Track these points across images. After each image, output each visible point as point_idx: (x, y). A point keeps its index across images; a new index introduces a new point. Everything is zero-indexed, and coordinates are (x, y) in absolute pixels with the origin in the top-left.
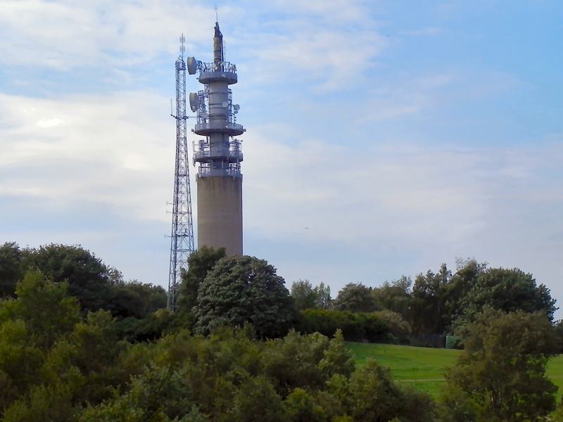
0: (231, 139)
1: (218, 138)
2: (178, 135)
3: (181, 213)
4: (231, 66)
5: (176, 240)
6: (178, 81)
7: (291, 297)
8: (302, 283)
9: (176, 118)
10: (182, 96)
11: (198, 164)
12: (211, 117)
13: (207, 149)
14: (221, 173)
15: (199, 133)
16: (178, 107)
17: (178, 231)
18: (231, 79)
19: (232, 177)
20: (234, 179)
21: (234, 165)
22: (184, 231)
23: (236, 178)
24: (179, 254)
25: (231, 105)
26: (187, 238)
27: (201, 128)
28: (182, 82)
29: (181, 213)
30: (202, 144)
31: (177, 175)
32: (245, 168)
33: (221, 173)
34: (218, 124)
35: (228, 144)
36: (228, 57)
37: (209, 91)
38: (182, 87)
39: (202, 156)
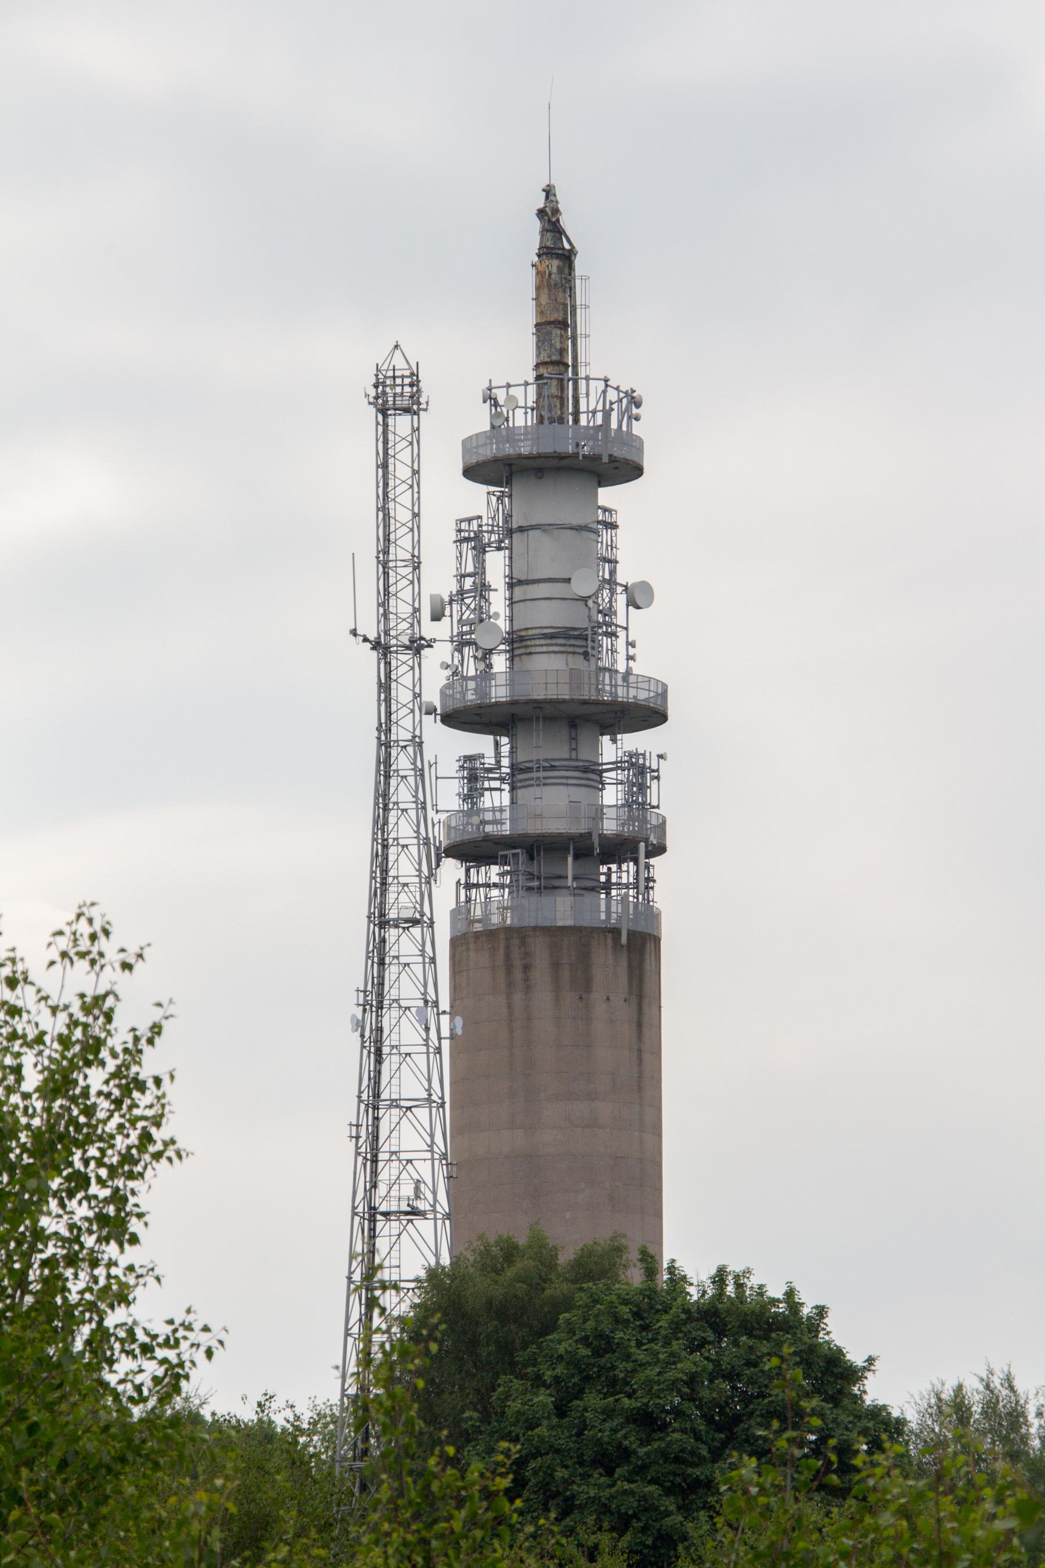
0: (609, 750)
1: (548, 747)
2: (385, 727)
3: (394, 1104)
4: (612, 395)
5: (373, 1236)
6: (384, 510)
7: (602, 734)
8: (959, 1406)
9: (376, 645)
10: (406, 542)
11: (452, 870)
12: (517, 643)
13: (497, 798)
14: (553, 929)
15: (458, 718)
16: (386, 595)
17: (382, 1189)
18: (612, 459)
19: (615, 932)
20: (624, 940)
21: (626, 873)
22: (408, 1190)
23: (631, 934)
24: (388, 1118)
25: (611, 582)
26: (416, 931)
27: (470, 696)
28: (401, 471)
29: (394, 1104)
30: (473, 774)
31: (381, 920)
32: (680, 891)
33: (553, 929)
34: (550, 675)
35: (592, 774)
36: (606, 354)
37: (508, 517)
38: (383, 721)
39: (471, 833)
